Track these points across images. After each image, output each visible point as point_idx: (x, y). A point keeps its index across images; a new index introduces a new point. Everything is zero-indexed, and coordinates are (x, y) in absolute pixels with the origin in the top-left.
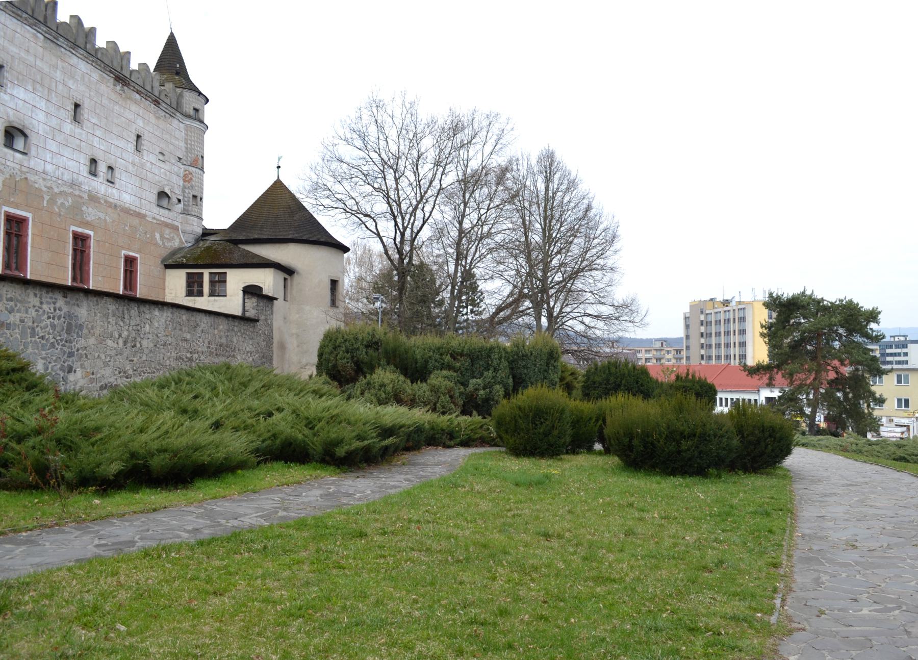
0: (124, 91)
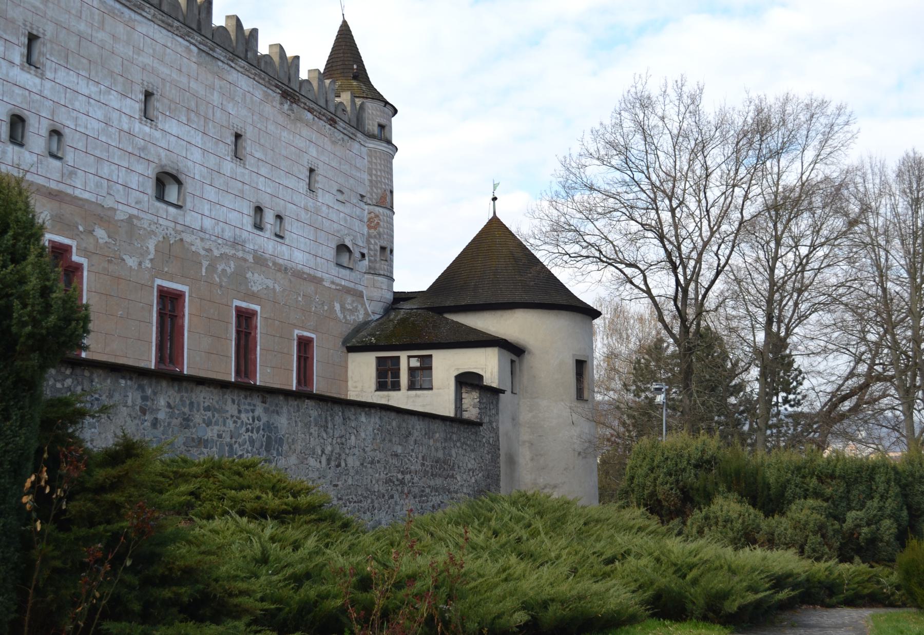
0: (292, 110)
